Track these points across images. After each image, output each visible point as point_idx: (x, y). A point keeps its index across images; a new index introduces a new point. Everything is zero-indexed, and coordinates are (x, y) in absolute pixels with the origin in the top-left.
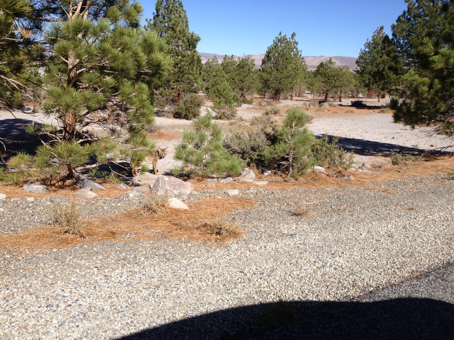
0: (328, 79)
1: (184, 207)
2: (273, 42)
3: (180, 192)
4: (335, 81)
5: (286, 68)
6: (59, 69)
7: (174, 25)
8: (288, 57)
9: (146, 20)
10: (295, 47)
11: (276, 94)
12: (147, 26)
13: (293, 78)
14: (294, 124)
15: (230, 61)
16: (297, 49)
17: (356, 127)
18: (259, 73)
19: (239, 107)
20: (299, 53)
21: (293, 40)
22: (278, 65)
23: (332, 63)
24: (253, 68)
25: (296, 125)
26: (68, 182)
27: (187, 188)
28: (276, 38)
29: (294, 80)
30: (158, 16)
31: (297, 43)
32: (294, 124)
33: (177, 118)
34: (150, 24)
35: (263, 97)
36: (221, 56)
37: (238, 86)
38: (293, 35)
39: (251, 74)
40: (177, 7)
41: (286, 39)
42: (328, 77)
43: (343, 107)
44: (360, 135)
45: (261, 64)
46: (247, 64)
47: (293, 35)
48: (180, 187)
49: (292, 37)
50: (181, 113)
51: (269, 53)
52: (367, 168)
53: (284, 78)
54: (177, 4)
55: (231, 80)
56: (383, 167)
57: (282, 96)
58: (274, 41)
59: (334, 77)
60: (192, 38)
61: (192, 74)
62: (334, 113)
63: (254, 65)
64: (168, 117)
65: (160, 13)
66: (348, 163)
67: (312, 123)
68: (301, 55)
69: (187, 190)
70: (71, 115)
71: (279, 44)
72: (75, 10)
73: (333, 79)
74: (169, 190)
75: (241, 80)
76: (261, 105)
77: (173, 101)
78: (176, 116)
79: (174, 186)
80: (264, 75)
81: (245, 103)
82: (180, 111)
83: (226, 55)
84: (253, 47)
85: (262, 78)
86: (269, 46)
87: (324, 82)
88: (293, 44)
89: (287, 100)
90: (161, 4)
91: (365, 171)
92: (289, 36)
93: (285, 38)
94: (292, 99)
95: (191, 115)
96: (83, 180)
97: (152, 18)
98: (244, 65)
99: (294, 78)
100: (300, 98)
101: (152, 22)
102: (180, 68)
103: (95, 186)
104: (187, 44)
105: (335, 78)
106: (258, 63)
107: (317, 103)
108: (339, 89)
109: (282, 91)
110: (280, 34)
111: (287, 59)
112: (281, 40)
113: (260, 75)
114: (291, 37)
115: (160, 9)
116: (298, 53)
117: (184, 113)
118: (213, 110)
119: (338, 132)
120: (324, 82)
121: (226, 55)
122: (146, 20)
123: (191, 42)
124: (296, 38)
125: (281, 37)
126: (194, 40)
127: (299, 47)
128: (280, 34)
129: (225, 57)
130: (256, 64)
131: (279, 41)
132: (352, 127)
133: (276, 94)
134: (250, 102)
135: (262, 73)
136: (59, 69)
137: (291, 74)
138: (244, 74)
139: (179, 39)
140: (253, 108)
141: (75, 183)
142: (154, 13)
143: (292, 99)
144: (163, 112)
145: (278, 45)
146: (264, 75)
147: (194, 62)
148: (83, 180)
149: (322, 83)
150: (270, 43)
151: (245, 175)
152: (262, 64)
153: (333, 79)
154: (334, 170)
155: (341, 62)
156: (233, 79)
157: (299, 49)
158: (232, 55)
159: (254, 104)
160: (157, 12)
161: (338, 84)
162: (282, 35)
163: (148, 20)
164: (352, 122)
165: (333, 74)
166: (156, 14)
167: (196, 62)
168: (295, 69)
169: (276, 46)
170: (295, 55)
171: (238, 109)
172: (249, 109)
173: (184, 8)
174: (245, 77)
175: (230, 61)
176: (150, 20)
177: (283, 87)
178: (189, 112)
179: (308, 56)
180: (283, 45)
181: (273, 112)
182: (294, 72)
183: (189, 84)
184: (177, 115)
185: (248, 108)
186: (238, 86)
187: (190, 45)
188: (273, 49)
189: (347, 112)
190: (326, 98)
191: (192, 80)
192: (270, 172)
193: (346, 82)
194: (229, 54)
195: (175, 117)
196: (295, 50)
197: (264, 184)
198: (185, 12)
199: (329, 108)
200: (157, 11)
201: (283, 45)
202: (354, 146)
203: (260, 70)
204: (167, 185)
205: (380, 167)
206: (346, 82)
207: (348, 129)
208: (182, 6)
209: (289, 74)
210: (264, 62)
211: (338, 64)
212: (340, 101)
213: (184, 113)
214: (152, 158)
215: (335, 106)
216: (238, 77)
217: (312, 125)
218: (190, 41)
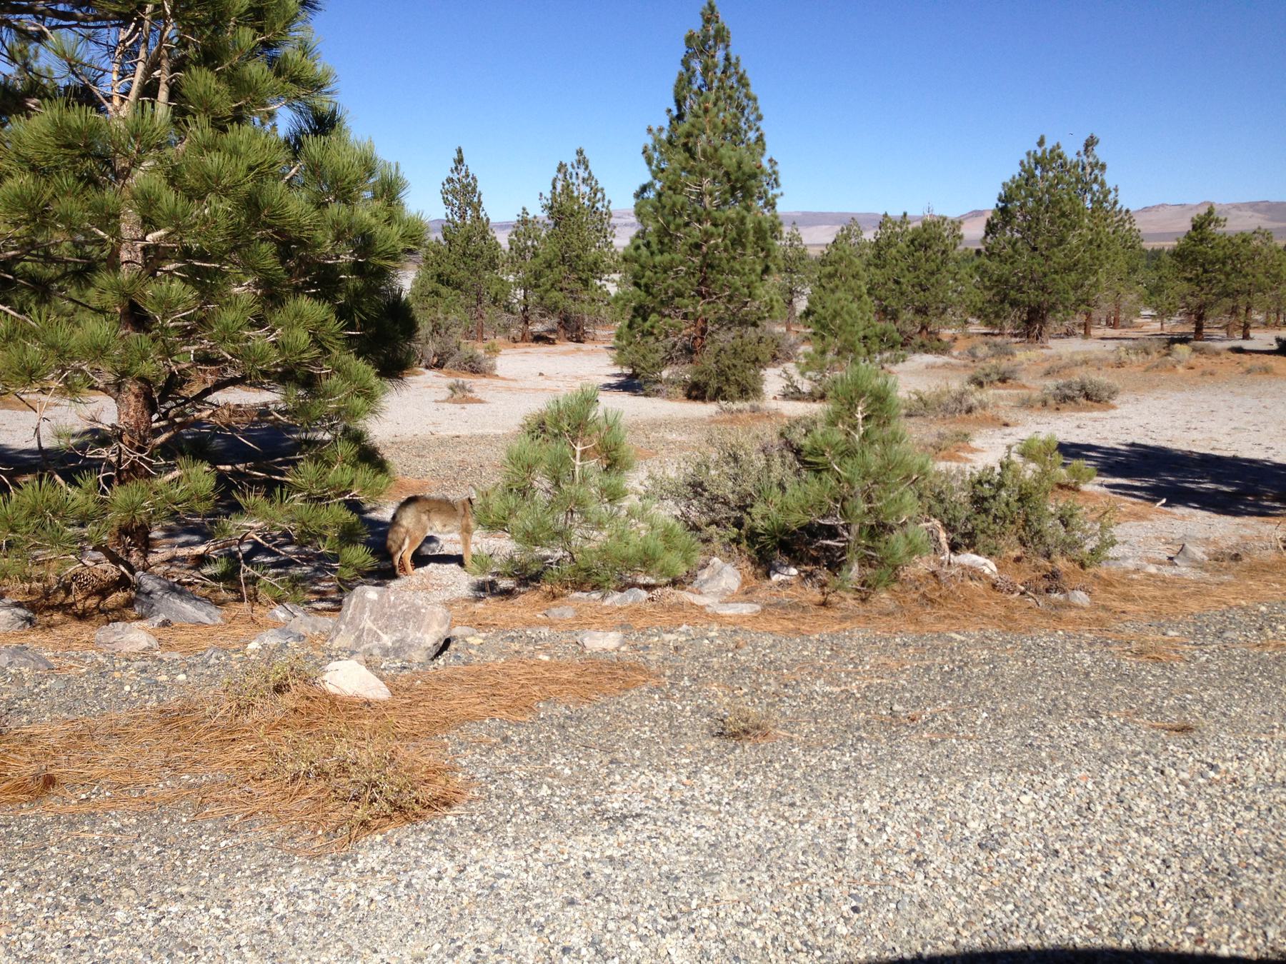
0: (1206, 271)
1: (377, 691)
2: (1019, 169)
3: (402, 640)
4: (1228, 275)
5: (1061, 241)
6: (439, 276)
7: (689, 135)
8: (1067, 208)
9: (650, 130)
10: (1096, 178)
11: (1033, 323)
12: (650, 146)
13: (1084, 271)
14: (859, 416)
15: (898, 229)
16: (1102, 184)
17: (1261, 418)
18: (977, 261)
19: (897, 362)
20: (1111, 197)
21: (1091, 159)
22: (1037, 235)
23: (1217, 221)
24: (955, 246)
25: (866, 419)
26: (117, 597)
27: (429, 625)
28: (1028, 154)
29: (1087, 278)
30: (680, 117)
31: (1103, 167)
32: (859, 416)
33: (696, 398)
34: (658, 141)
35: (997, 331)
36: (869, 217)
37: (912, 301)
38: (1090, 143)
39: (951, 266)
40: (732, 87)
41: (1060, 157)
42: (1203, 265)
43: (1245, 357)
44: (1267, 443)
45: (983, 233)
46: (939, 237)
47: (1090, 143)
48: (406, 620)
49: (1086, 150)
50: (706, 384)
51: (1006, 199)
52: (1194, 560)
53: (1056, 272)
54: (733, 80)
55: (891, 285)
56: (1246, 560)
57: (1053, 325)
58: (1022, 163)
59: (1224, 264)
60: (739, 167)
61: (738, 273)
62: (1203, 374)
63: (961, 237)
64: (669, 397)
65: (686, 109)
66: (1090, 544)
67: (1113, 407)
68: (1116, 203)
69: (426, 632)
70: (132, 398)
71: (1038, 172)
72: (127, 94)
73: (1220, 270)
74: (370, 630)
75: (921, 285)
76: (974, 355)
77: (690, 351)
78: (694, 393)
79: (391, 616)
80: (992, 265)
81: (926, 352)
82: (702, 378)
83: (886, 215)
84: (958, 189)
85: (982, 271)
86: (1007, 179)
87: (1189, 280)
88: (1088, 170)
89: (1072, 340)
90: (690, 82)
91: (1183, 569)
92: (1071, 152)
93: (1056, 154)
94: (1087, 335)
95: (733, 390)
96: (151, 592)
97: (666, 124)
98: (927, 241)
99: (1090, 270)
100: (1115, 333)
101: (664, 136)
102: (705, 256)
103: (183, 613)
104: (727, 187)
105: (1228, 268)
106: (974, 232)
107: (1155, 345)
108: (1241, 299)
109: (1048, 311)
110: (1041, 143)
111: (1063, 215)
112: (1047, 160)
113: (977, 268)
114: (1082, 149)
115: (685, 98)
116: (1105, 196)
117: (714, 384)
118: (803, 374)
119: (1195, 435)
120: (1189, 280)
121: (886, 215)
122: (650, 130)
123: (737, 180)
124: (1100, 152)
125: (1044, 151)
126: (744, 174)
127: (1110, 179)
128: (1041, 143)
129: (884, 221)
130: (966, 237)
131: (1037, 163)
132: (1250, 418)
133: (1029, 322)
134: (943, 350)
135: (986, 261)
136: (439, 276)
137: (1078, 261)
138: (927, 267)
139: (702, 173)
140: (944, 366)
141: (130, 603)
142: (670, 111)
143: (1087, 335)
144: (657, 382)
145: (1034, 176)
146: (992, 265)
147: (746, 237)
148: (149, 594)
149: (1185, 284)
150: (1011, 171)
151: (706, 581)
152: (987, 234)
153: (1220, 270)
154: (1037, 568)
155: (1272, 220)
156: (897, 282)
157: (1110, 184)
158: (905, 214)
159: (955, 353)
160: (679, 107)
161: (1235, 286)
162: (1048, 145)
163: (655, 130)
164: (1256, 402)
165: (1221, 254)
166: (675, 112)
167: (751, 238)
168: (1091, 242)
169: (1029, 177)
170: (1098, 203)
171: (895, 368)
172: (933, 367)
173: (753, 90)
174: (932, 274)
175: (898, 229)
176: (661, 130)
177: (1053, 300)
178: (727, 380)
179: (1163, 205)
180: (1051, 174)
181: (995, 377)
182: (1088, 254)
183: (729, 301)
184: (696, 392)
185: (930, 367)
186: (912, 301)
187: (733, 189)
188: (1018, 187)
189: (1249, 371)
190: (1199, 329)
191: (737, 289)
192: (794, 571)
193: (1261, 278)
194: (895, 213)
195: (690, 397)
196: (1095, 187)
197: (744, 612)
198: (755, 100)
199: (1195, 360)
200: (679, 102)
201: (1051, 174)
202: (1215, 480)
203: (978, 252)
204: (367, 614)
205: (1236, 557)
206: (1261, 278)
207: (1233, 425)
208: (746, 85)
209: (1070, 262)
210: (991, 228)
211: (1236, 225)
212: (1246, 337)
213: (714, 384)
214: (457, 523)
215: (1218, 354)
216: (910, 276)
217: (1112, 412)
218: (733, 177)
